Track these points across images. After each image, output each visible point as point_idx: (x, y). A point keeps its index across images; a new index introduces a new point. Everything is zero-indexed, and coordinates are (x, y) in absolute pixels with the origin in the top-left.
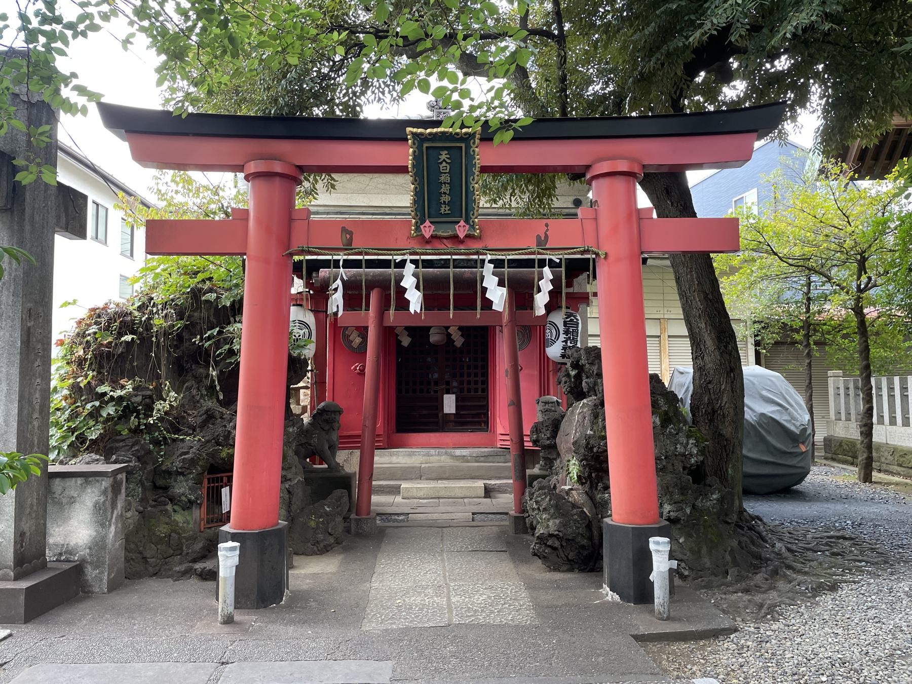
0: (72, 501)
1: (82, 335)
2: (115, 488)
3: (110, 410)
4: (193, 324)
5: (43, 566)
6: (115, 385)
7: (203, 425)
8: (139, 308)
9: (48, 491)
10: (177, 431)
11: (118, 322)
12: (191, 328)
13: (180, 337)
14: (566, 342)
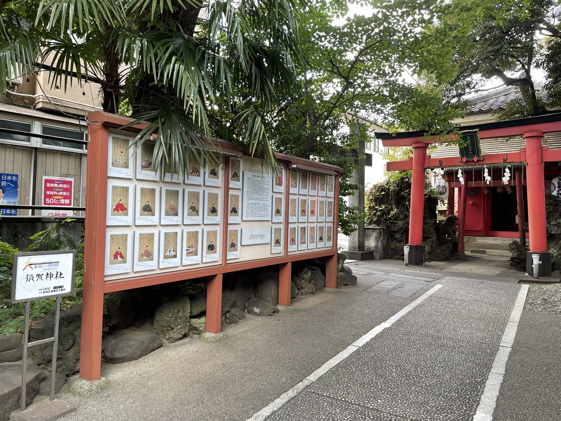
0: (370, 235)
1: (371, 192)
2: (380, 233)
3: (379, 213)
4: (402, 189)
5: (364, 250)
6: (380, 206)
7: (404, 219)
8: (387, 184)
9: (365, 233)
10: (397, 220)
11: (381, 188)
12: (401, 190)
13: (398, 192)
14: (559, 191)
